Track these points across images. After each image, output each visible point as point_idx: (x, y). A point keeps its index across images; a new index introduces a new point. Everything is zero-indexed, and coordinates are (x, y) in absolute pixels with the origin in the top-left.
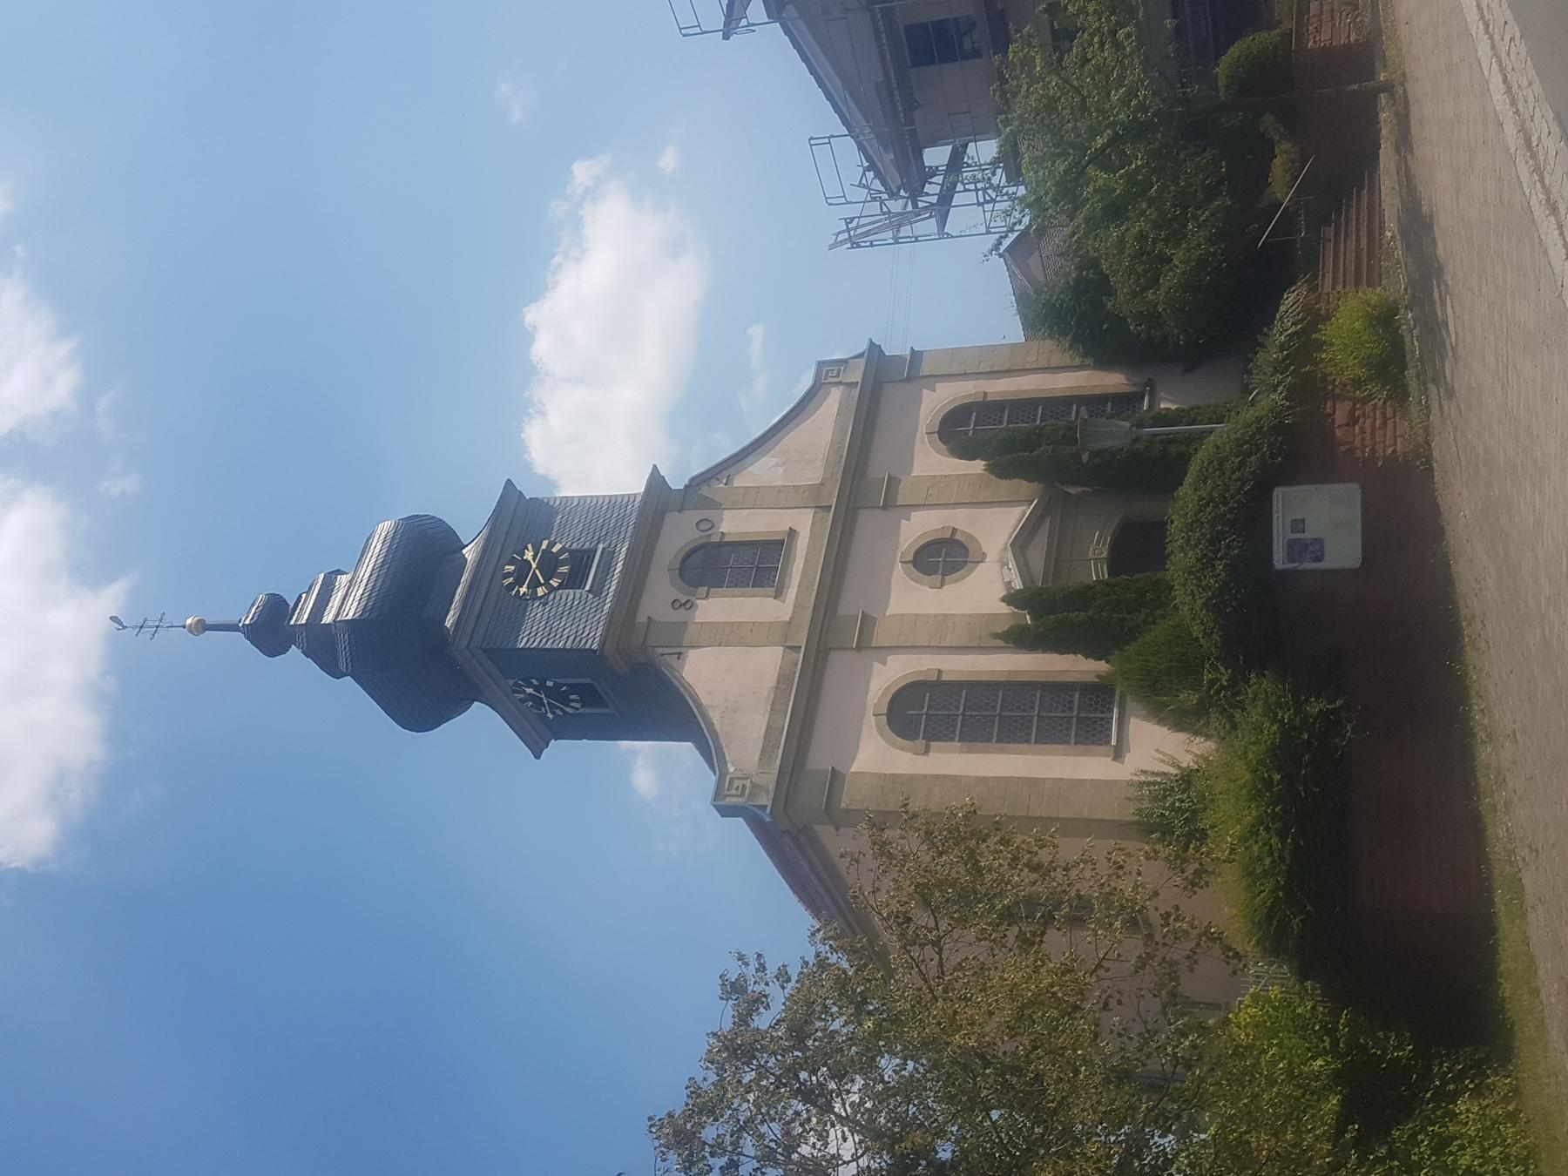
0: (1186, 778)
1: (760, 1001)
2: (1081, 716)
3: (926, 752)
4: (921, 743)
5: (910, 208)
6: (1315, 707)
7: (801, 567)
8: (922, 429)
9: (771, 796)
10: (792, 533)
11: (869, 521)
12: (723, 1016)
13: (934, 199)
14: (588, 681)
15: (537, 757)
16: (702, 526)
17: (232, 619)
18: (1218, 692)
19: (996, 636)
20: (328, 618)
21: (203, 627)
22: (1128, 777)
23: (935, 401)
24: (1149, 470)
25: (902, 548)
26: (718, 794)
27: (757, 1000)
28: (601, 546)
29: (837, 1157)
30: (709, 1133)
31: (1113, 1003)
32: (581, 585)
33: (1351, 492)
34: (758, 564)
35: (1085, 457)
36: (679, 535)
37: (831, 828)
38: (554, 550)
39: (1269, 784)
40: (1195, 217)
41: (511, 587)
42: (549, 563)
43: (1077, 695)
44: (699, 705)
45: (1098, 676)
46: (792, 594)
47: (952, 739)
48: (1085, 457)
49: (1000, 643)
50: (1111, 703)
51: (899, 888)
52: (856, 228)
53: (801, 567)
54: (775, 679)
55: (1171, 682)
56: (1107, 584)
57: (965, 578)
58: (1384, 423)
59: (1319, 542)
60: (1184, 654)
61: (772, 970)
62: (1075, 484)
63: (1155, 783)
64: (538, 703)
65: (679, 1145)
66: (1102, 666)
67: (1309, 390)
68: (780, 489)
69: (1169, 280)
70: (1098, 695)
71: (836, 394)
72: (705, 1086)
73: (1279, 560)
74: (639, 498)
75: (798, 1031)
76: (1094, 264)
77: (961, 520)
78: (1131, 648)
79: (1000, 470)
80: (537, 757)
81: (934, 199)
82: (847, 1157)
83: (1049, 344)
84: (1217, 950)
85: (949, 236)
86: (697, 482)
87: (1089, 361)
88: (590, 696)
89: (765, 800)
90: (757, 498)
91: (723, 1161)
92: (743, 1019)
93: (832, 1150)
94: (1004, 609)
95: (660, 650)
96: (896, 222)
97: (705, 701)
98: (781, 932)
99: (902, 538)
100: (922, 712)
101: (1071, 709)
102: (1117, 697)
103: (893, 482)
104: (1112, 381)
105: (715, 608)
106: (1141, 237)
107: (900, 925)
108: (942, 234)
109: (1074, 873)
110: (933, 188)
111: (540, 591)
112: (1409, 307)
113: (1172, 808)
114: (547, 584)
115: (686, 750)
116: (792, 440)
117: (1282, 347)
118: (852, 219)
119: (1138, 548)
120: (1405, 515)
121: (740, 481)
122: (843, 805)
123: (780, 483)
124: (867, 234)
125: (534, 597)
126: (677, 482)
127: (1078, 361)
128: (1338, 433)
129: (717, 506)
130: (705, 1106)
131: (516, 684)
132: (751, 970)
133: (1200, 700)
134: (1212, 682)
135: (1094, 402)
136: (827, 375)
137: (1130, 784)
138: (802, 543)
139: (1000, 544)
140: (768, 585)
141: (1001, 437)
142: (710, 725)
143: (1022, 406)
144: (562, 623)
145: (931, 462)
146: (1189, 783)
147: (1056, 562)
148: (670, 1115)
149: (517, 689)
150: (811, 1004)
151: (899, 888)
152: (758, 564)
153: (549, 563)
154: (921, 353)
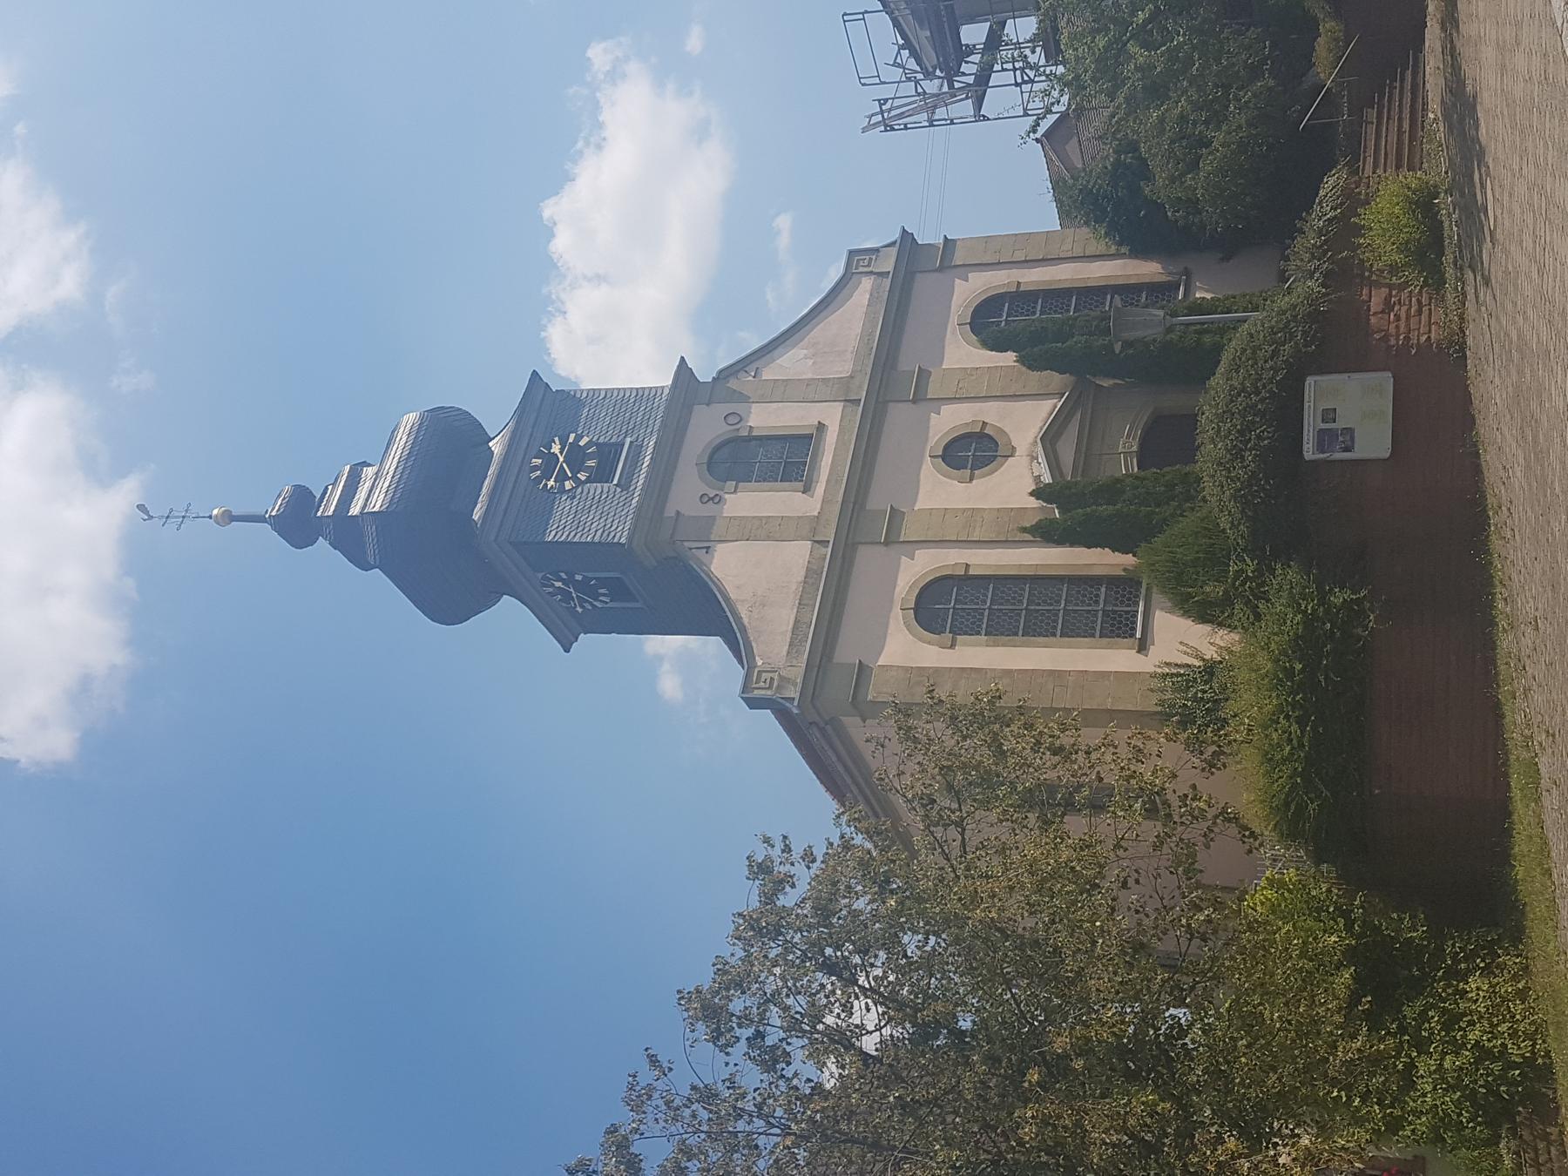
0: (1210, 669)
1: (788, 880)
2: (1111, 612)
3: (952, 646)
5: (945, 89)
6: (1338, 598)
7: (829, 460)
8: (954, 319)
9: (799, 689)
10: (821, 427)
11: (899, 415)
12: (748, 897)
13: (971, 80)
15: (567, 651)
16: (732, 420)
17: (259, 511)
18: (1243, 584)
19: (1024, 530)
20: (355, 510)
21: (229, 517)
22: (1152, 669)
23: (968, 290)
24: (1186, 361)
25: (932, 442)
26: (746, 687)
27: (781, 882)
28: (628, 440)
29: (861, 1027)
31: (1131, 882)
32: (609, 479)
33: (1385, 380)
34: (788, 458)
35: (1118, 347)
36: (707, 427)
37: (858, 719)
38: (582, 443)
39: (1290, 673)
41: (538, 480)
42: (576, 457)
44: (727, 599)
46: (820, 489)
47: (978, 633)
48: (1118, 347)
49: (1028, 537)
52: (890, 110)
53: (829, 460)
54: (803, 573)
56: (1137, 478)
58: (1420, 312)
59: (1349, 431)
62: (1107, 375)
64: (567, 597)
66: (1129, 560)
67: (1344, 273)
68: (809, 382)
70: (1124, 586)
71: (867, 283)
72: (732, 961)
73: (1309, 452)
74: (666, 391)
75: (824, 911)
76: (1133, 147)
77: (992, 414)
78: (1158, 541)
79: (1031, 362)
80: (567, 651)
81: (971, 80)
82: (871, 1027)
84: (1233, 830)
85: (986, 118)
86: (725, 374)
88: (619, 590)
89: (793, 692)
90: (785, 391)
91: (750, 1032)
92: (769, 898)
93: (856, 1020)
94: (1033, 503)
96: (931, 104)
98: (812, 818)
100: (946, 606)
101: (1097, 602)
102: (1143, 591)
103: (924, 374)
104: (1148, 270)
105: (744, 502)
106: (1183, 118)
107: (924, 806)
108: (980, 117)
109: (1094, 756)
110: (970, 68)
111: (568, 485)
112: (1449, 192)
114: (575, 478)
115: (714, 645)
117: (1320, 233)
118: (886, 100)
119: (1168, 440)
120: (1437, 399)
121: (767, 375)
122: (870, 697)
123: (810, 376)
125: (562, 491)
126: (704, 373)
127: (1113, 249)
128: (1373, 320)
129: (745, 399)
130: (732, 980)
131: (544, 578)
132: (777, 851)
133: (1226, 592)
134: (1238, 573)
135: (1128, 291)
137: (1153, 676)
139: (1030, 439)
142: (738, 619)
143: (1055, 296)
144: (591, 516)
145: (963, 354)
146: (1212, 674)
147: (1085, 454)
148: (698, 991)
149: (546, 582)
152: (788, 458)
153: (576, 457)
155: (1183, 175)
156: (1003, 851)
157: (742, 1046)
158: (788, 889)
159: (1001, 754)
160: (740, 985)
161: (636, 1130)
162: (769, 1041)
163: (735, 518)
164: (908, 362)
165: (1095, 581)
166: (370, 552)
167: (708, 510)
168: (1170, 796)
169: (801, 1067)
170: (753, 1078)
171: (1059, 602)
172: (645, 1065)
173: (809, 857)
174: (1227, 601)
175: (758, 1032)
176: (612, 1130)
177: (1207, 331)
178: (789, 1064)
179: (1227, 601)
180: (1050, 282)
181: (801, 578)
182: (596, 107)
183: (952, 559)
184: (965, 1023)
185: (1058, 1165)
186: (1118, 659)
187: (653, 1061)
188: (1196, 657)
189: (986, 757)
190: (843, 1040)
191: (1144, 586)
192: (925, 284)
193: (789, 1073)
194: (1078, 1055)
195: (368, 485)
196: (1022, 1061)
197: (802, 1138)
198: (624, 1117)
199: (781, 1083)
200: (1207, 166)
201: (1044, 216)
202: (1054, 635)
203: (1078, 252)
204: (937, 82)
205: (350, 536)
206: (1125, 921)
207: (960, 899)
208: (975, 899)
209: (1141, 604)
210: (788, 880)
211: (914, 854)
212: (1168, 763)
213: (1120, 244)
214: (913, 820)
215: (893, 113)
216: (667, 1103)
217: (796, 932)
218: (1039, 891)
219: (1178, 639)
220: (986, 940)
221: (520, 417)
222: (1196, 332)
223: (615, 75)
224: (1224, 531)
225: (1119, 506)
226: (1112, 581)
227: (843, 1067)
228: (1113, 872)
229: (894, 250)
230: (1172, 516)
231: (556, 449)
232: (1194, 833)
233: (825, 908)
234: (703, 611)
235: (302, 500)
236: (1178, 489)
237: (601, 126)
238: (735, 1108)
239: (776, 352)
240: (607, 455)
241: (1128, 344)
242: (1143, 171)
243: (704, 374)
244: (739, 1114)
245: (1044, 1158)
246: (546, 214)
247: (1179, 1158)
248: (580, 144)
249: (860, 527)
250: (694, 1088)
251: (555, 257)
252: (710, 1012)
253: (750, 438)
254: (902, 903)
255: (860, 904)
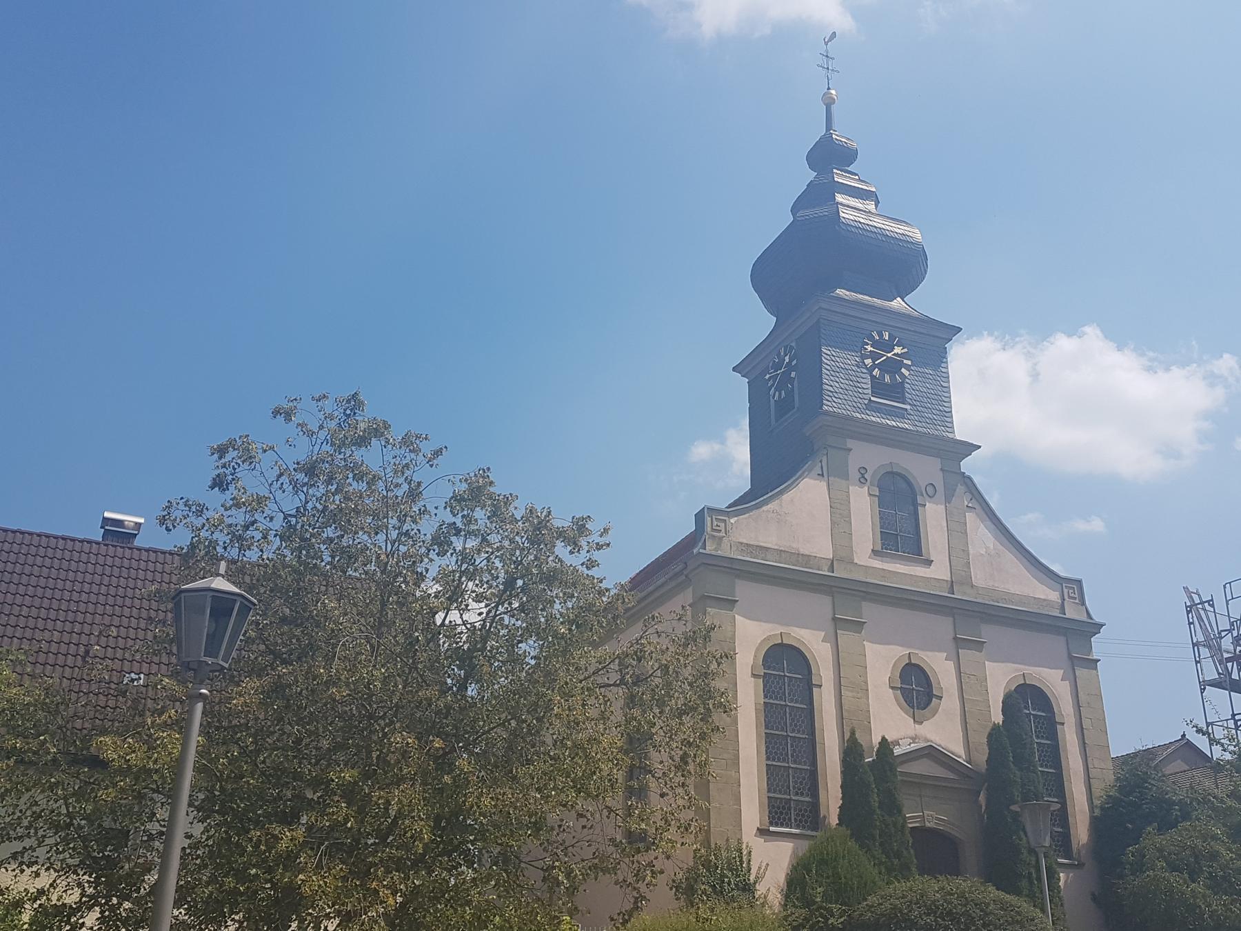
0: (748, 888)
1: (576, 547)
2: (790, 806)
3: (754, 675)
4: (762, 672)
5: (1226, 655)
7: (901, 570)
8: (1028, 670)
9: (713, 553)
10: (929, 562)
11: (943, 626)
12: (561, 521)
14: (797, 405)
15: (734, 369)
16: (930, 490)
19: (853, 733)
20: (839, 198)
21: (829, 103)
22: (745, 840)
23: (1054, 681)
24: (1006, 863)
25: (922, 654)
27: (575, 544)
28: (908, 407)
29: (467, 609)
30: (479, 514)
31: (583, 821)
32: (874, 394)
34: (901, 537)
35: (1014, 808)
36: (923, 470)
40: (1233, 902)
41: (871, 338)
42: (893, 366)
43: (807, 799)
44: (781, 493)
45: (825, 817)
46: (877, 564)
47: (766, 697)
48: (1014, 808)
49: (847, 736)
50: (804, 827)
51: (663, 652)
52: (1204, 609)
53: (901, 570)
54: (807, 553)
55: (828, 877)
56: (903, 826)
57: (901, 705)
60: (852, 889)
61: (596, 555)
63: (741, 862)
64: (777, 367)
65: (471, 490)
66: (834, 820)
68: (966, 552)
69: (1175, 880)
70: (811, 817)
71: (1054, 596)
72: (511, 508)
74: (950, 435)
75: (551, 578)
76: (1186, 816)
77: (949, 704)
78: (851, 844)
79: (995, 735)
80: (734, 369)
82: (465, 617)
83: (1111, 778)
85: (1202, 691)
86: (968, 482)
87: (1097, 812)
88: (784, 407)
89: (710, 548)
91: (459, 524)
92: (561, 534)
93: (473, 605)
94: (876, 740)
95: (824, 459)
97: (786, 497)
98: (616, 568)
99: (929, 653)
100: (786, 668)
101: (797, 794)
102: (809, 833)
103: (979, 645)
104: (1081, 832)
106: (1214, 856)
107: (636, 653)
109: (680, 790)
111: (868, 362)
113: (723, 876)
114: (874, 366)
116: (1010, 559)
118: (1212, 606)
119: (937, 852)
121: (970, 517)
123: (971, 551)
124: (1200, 619)
125: (863, 357)
127: (1097, 802)
129: (948, 500)
131: (792, 348)
132: (598, 540)
135: (1062, 817)
136: (1073, 587)
137: (740, 841)
138: (920, 571)
139: (929, 736)
140: (883, 544)
141: (1026, 727)
142: (766, 502)
143: (1054, 755)
144: (843, 380)
145: (999, 678)
146: (744, 890)
147: (920, 783)
148: (491, 483)
149: (788, 350)
150: (574, 585)
151: (663, 652)
152: (901, 537)
153: (893, 366)
154: (1096, 668)
155: (1164, 857)
156: (603, 717)
157: (450, 519)
158: (569, 548)
159: (681, 714)
160: (495, 515)
161: (388, 442)
162: (453, 539)
163: (848, 496)
164: (988, 632)
165: (814, 790)
166: (807, 212)
167: (854, 474)
168: (652, 854)
169: (435, 565)
170: (427, 528)
171: (795, 762)
172: (436, 447)
173: (591, 564)
174: (808, 903)
175: (460, 530)
176: (387, 426)
177: (1031, 883)
178: (438, 554)
179: (808, 903)
180: (1066, 751)
181: (802, 551)
182: (1183, 365)
183: (825, 673)
184: (472, 691)
185: (370, 766)
186: (752, 813)
187: (438, 453)
188: (757, 877)
189: (678, 702)
190: (454, 597)
191: (814, 833)
192: (1057, 644)
193: (432, 555)
194: (454, 778)
195: (860, 206)
196: (447, 735)
197: (384, 567)
198: (396, 434)
199: (423, 550)
200: (1174, 879)
201: (1122, 743)
202: (768, 759)
203: (1093, 773)
204: (1232, 648)
205: (819, 194)
206: (552, 818)
207: (566, 683)
208: (567, 695)
209: (797, 831)
210: (576, 547)
211: (595, 645)
212: (679, 852)
213: (1102, 808)
214: (622, 643)
215: (1202, 612)
216: (407, 466)
217: (534, 559)
218: (575, 745)
219: (772, 862)
220: (536, 704)
221: (923, 321)
222: (1030, 874)
223: (1212, 380)
224: (866, 900)
225: (878, 811)
226: (815, 806)
227: (436, 597)
228: (591, 806)
229: (1084, 618)
230: (874, 857)
231: (898, 350)
232: (625, 872)
233: (554, 578)
234: (772, 472)
235: (846, 157)
236: (896, 862)
237: (1167, 369)
238: (405, 516)
239: (989, 523)
240: (896, 391)
241: (1015, 817)
242: (1167, 825)
243: (966, 465)
244: (402, 520)
245: (374, 755)
246: (1087, 329)
247: (381, 860)
248: (1151, 354)
249: (845, 597)
250: (419, 484)
251: (1052, 339)
252: (475, 493)
253: (915, 505)
254: (562, 638)
255: (557, 606)
